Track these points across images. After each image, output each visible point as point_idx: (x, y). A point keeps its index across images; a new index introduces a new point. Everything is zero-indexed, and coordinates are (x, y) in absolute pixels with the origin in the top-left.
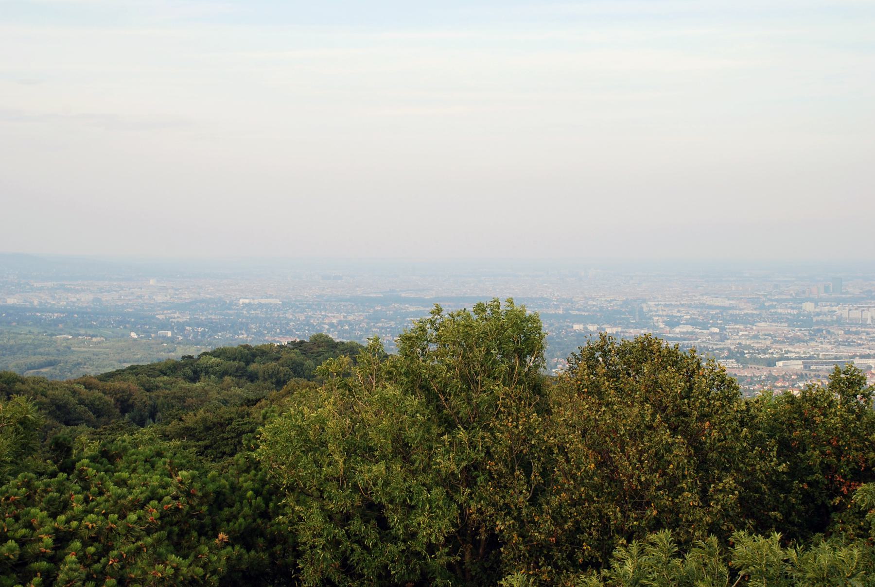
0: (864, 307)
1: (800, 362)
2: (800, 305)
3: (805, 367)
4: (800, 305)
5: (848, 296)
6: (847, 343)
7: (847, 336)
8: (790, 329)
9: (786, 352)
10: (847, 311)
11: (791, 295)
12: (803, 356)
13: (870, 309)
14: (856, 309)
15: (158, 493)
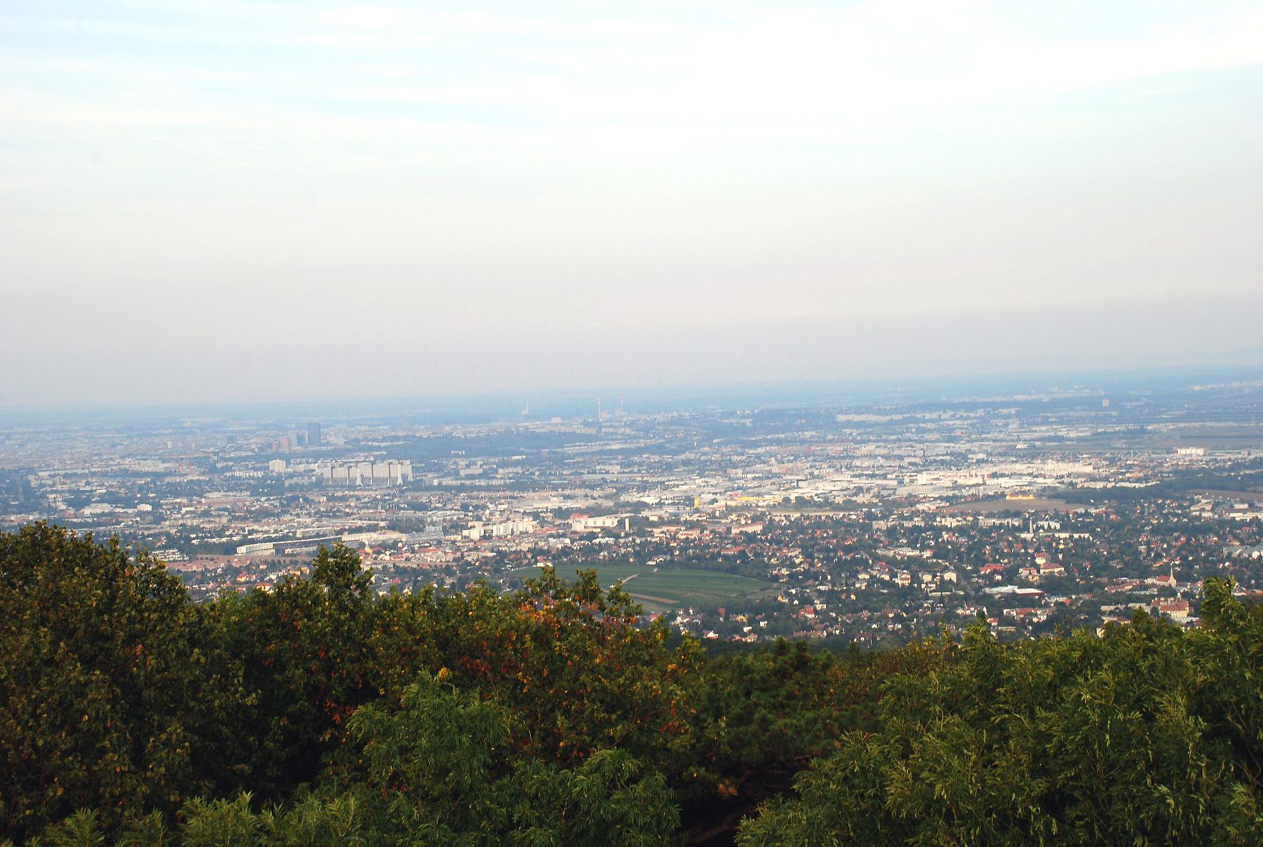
1: (270, 545)
2: (266, 465)
3: (278, 551)
4: (266, 465)
5: (330, 448)
7: (331, 504)
8: (253, 499)
9: (251, 532)
11: (253, 450)
12: (274, 536)
14: (341, 466)
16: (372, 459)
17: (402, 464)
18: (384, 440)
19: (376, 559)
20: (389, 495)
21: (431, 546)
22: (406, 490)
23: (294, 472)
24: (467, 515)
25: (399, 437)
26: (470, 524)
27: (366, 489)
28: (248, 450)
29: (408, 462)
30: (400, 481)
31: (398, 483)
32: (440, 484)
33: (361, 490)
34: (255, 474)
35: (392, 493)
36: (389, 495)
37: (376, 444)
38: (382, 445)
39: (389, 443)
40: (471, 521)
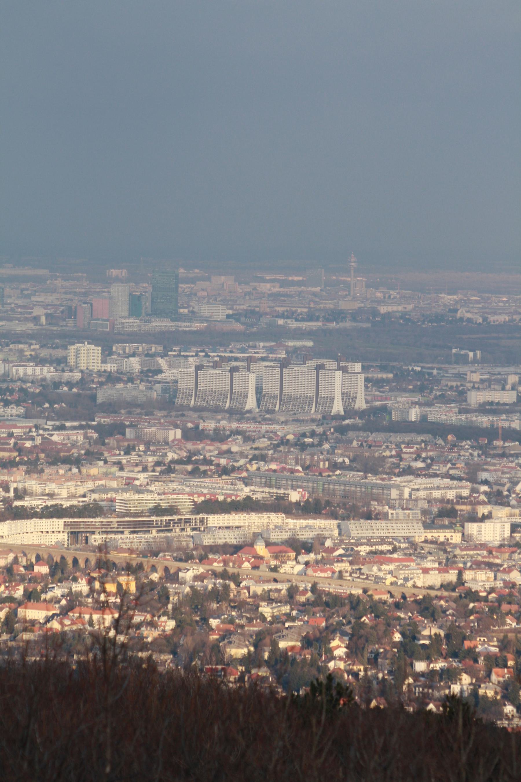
0: (236, 359)
1: (58, 523)
2: (59, 353)
3: (74, 535)
4: (59, 353)
5: (196, 326)
6: (189, 468)
7: (190, 446)
8: (31, 423)
9: (20, 495)
10: (192, 370)
11: (36, 319)
12: (66, 504)
13: (253, 366)
14: (216, 365)
15: (187, 593)
16: (283, 355)
17: (344, 370)
18: (311, 317)
19: (275, 569)
20: (313, 434)
21: (395, 550)
22: (349, 428)
23: (119, 372)
24: (478, 492)
25: (341, 312)
26: (482, 510)
27: (264, 419)
28: (26, 320)
29: (358, 367)
30: (338, 407)
31: (334, 411)
32: (424, 418)
33: (254, 420)
34: (38, 369)
35: (320, 430)
36: (313, 434)
37: (293, 324)
38: (306, 325)
39: (391, 364)
40: (483, 503)
